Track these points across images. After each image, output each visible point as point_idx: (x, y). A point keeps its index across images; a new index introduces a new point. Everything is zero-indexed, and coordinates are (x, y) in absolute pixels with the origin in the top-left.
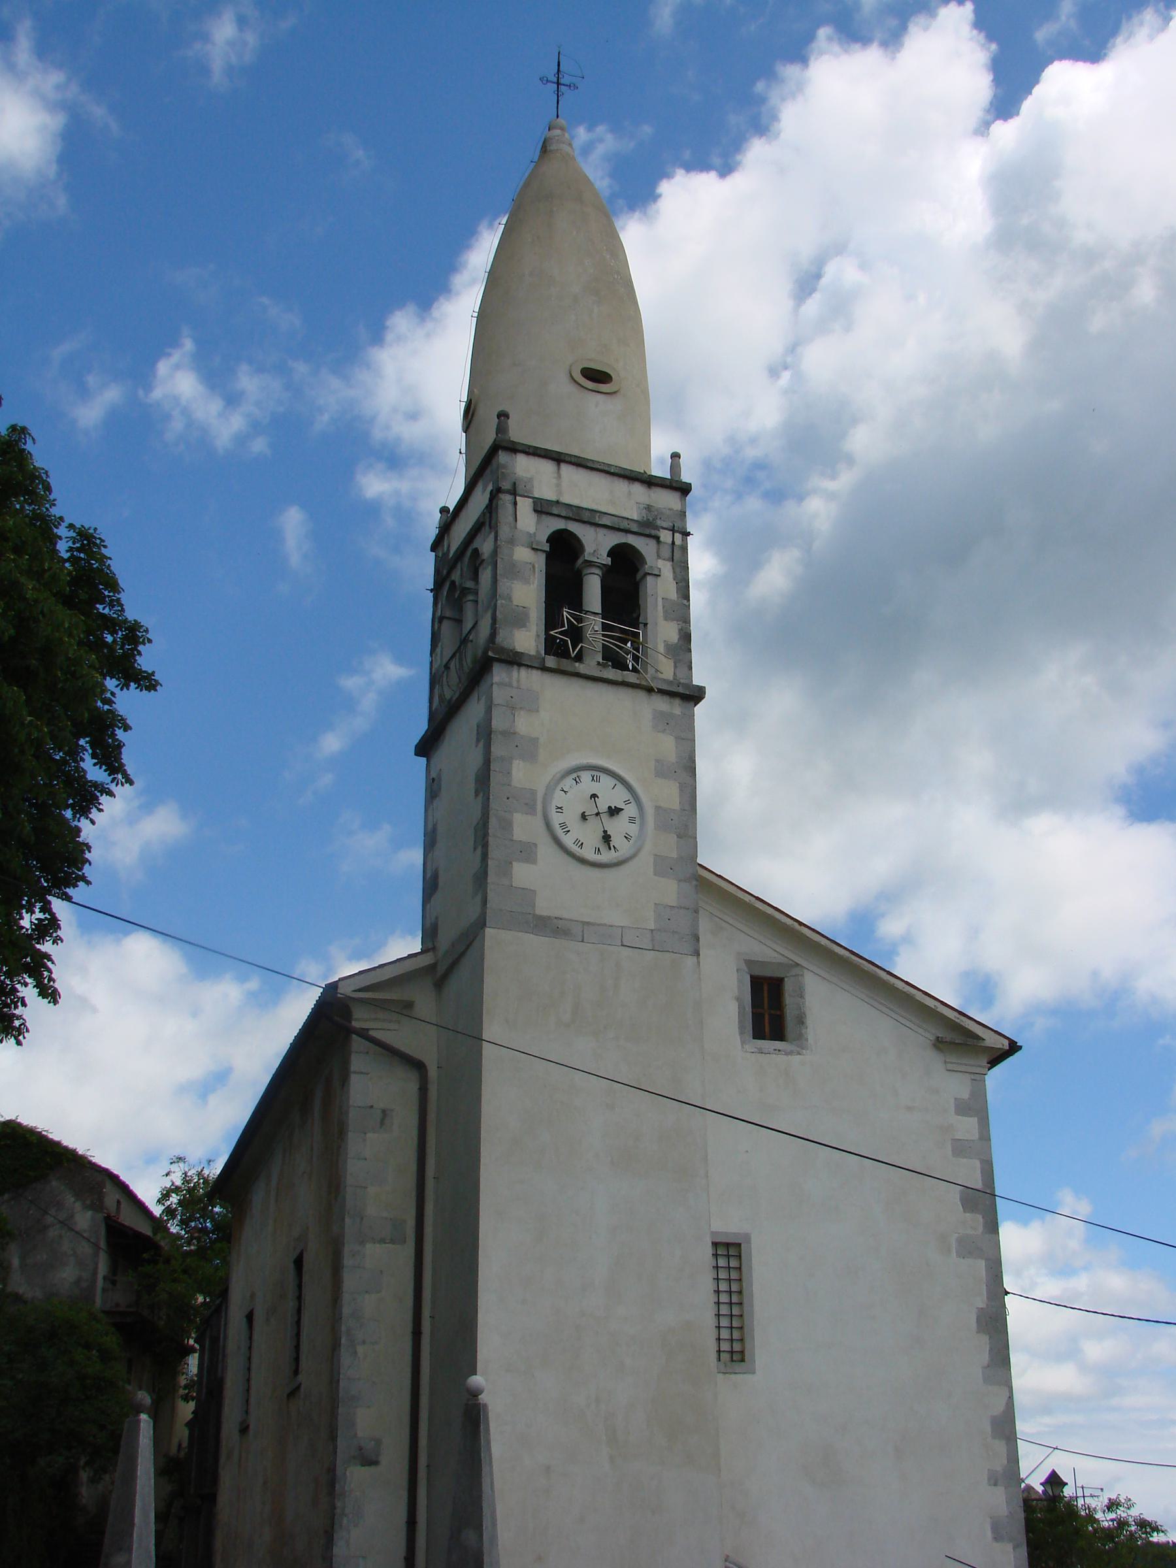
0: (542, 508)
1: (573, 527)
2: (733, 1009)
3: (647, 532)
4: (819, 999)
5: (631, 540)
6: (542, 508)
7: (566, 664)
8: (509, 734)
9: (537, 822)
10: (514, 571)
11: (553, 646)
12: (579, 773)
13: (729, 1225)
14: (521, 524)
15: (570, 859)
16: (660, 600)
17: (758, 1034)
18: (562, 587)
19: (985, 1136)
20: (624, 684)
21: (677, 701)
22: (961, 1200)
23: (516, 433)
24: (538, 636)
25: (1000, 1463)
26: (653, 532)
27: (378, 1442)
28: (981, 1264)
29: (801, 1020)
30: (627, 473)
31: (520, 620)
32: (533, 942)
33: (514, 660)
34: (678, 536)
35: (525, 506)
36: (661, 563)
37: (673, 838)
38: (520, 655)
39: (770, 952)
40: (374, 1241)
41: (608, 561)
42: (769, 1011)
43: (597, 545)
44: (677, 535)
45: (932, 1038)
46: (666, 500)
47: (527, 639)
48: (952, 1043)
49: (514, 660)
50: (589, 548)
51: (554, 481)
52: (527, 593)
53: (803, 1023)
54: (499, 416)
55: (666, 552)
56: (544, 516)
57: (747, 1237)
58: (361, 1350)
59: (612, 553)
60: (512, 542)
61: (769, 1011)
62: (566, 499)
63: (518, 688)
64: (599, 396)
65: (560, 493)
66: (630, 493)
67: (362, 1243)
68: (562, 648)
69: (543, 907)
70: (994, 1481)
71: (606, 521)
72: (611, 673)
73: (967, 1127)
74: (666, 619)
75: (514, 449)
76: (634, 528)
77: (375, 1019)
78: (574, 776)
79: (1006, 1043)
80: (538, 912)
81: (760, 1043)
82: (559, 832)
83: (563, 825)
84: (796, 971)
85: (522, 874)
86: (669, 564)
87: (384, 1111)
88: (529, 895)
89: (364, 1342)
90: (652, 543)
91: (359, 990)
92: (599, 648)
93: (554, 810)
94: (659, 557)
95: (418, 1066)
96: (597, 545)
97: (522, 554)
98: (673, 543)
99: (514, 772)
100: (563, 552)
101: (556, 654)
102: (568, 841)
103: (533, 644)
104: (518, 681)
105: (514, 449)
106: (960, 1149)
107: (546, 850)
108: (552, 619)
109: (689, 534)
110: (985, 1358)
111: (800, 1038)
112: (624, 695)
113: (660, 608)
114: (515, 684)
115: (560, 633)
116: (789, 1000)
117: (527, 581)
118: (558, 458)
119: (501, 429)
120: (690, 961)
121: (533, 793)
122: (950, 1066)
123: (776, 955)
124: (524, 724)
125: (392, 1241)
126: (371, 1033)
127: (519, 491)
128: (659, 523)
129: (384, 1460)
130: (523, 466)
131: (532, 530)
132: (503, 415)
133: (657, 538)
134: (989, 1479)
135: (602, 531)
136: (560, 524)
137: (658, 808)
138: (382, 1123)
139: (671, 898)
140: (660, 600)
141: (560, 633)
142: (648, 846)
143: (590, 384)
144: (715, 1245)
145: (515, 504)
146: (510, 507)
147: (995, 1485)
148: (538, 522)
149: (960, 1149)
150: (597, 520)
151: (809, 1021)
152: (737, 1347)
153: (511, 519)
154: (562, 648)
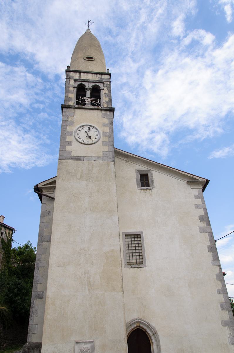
0: (75, 80)
1: (83, 83)
2: (135, 181)
4: (156, 176)
9: (73, 137)
11: (78, 103)
12: (84, 127)
15: (78, 143)
16: (104, 94)
19: (204, 202)
20: (94, 109)
22: (199, 218)
25: (220, 287)
28: (207, 234)
29: (153, 182)
34: (108, 83)
37: (107, 138)
39: (143, 168)
42: (145, 180)
43: (89, 86)
45: (186, 182)
46: (106, 77)
48: (191, 182)
53: (153, 182)
55: (105, 85)
56: (76, 82)
57: (142, 233)
61: (145, 180)
64: (90, 61)
66: (97, 76)
69: (74, 154)
70: (219, 292)
71: (91, 81)
72: (93, 107)
73: (199, 201)
77: (51, 192)
78: (82, 127)
79: (205, 180)
82: (82, 142)
84: (151, 171)
87: (49, 211)
90: (102, 84)
91: (44, 185)
92: (90, 103)
96: (89, 86)
98: (107, 84)
106: (197, 206)
107: (75, 143)
108: (77, 98)
109: (111, 82)
110: (212, 258)
111: (153, 185)
112: (95, 111)
113: (104, 95)
116: (150, 178)
122: (192, 188)
123: (145, 168)
126: (47, 195)
127: (71, 78)
130: (72, 74)
134: (218, 292)
135: (90, 83)
136: (80, 83)
138: (49, 214)
140: (104, 94)
142: (101, 140)
143: (87, 59)
144: (126, 235)
145: (70, 80)
147: (220, 293)
149: (197, 206)
151: (155, 181)
152: (141, 260)
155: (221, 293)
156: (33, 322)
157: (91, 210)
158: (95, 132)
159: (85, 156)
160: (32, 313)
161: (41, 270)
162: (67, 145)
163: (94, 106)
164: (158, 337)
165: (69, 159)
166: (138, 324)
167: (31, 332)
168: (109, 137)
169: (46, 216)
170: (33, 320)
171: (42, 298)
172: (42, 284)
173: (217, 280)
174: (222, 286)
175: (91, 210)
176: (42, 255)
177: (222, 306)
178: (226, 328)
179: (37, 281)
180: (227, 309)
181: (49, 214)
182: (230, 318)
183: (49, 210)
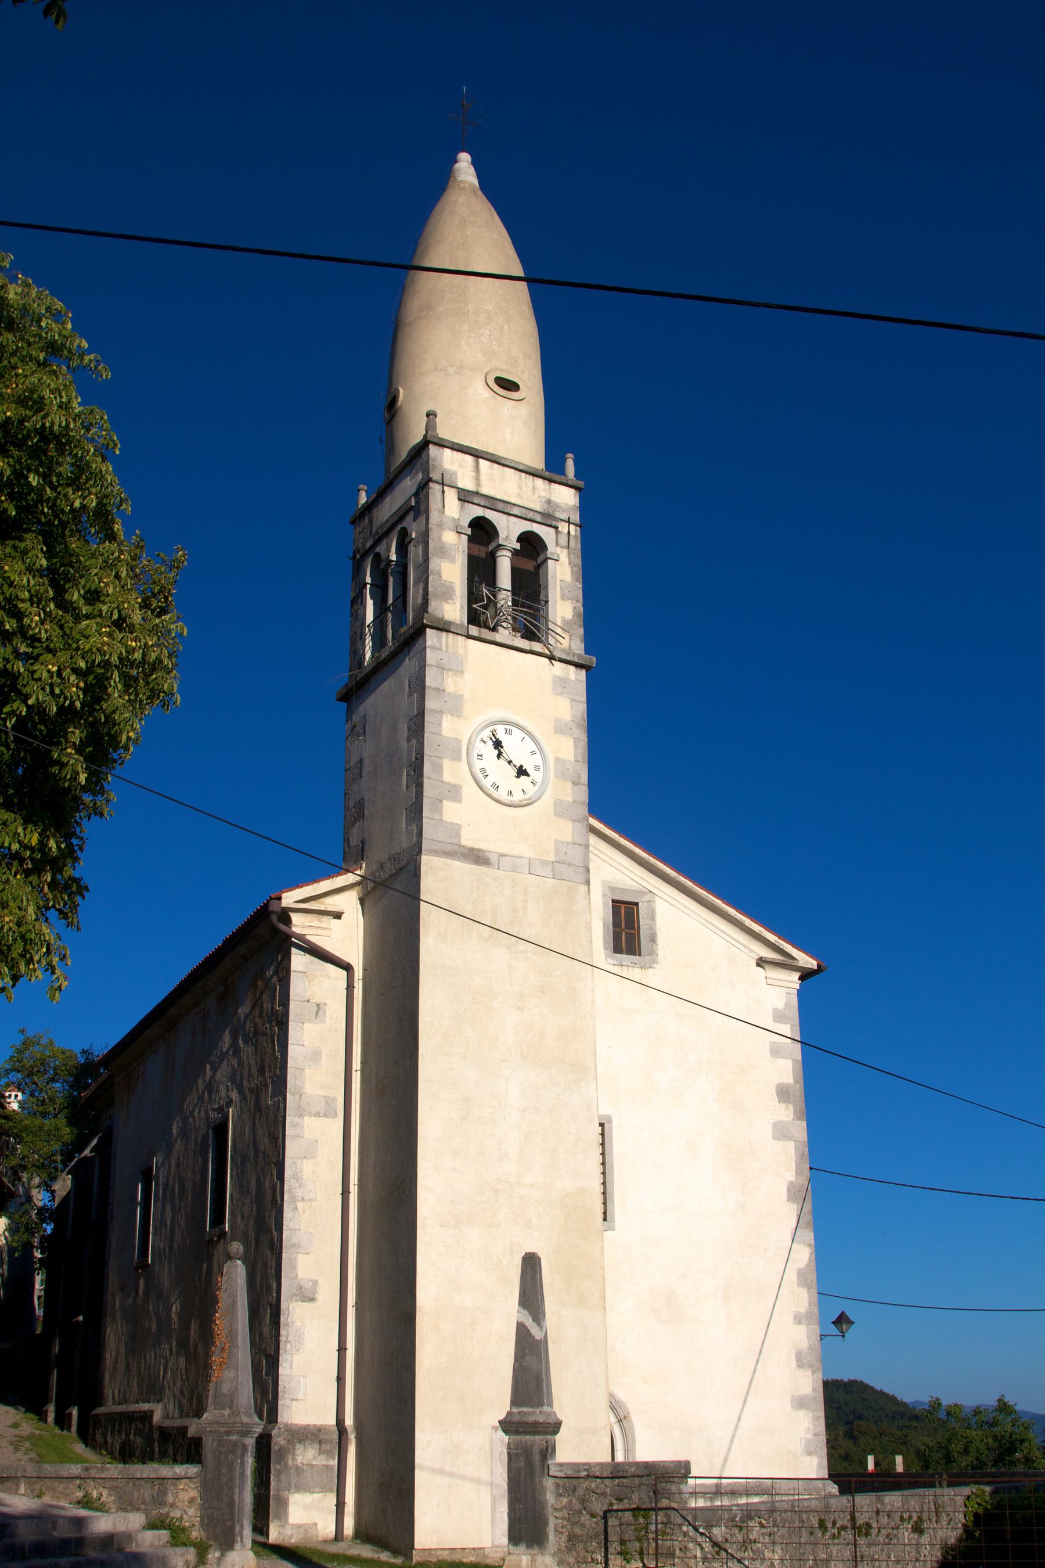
0: (465, 497)
1: (490, 515)
3: (548, 523)
5: (536, 528)
6: (465, 497)
7: (486, 634)
8: (440, 690)
10: (444, 552)
11: (474, 618)
13: (605, 1110)
14: (447, 511)
17: (617, 949)
18: (481, 570)
21: (572, 668)
23: (444, 432)
24: (462, 607)
26: (554, 523)
27: (315, 1283)
29: (653, 939)
30: (532, 471)
31: (447, 594)
32: (460, 867)
33: (444, 627)
35: (451, 496)
36: (558, 550)
38: (450, 623)
40: (310, 1115)
41: (518, 546)
44: (572, 526)
47: (454, 609)
49: (444, 627)
50: (502, 535)
51: (474, 474)
52: (450, 571)
54: (428, 415)
55: (563, 540)
58: (300, 1205)
59: (520, 539)
60: (440, 526)
62: (485, 490)
63: (447, 652)
65: (478, 484)
67: (301, 1116)
68: (480, 616)
69: (468, 839)
74: (563, 598)
75: (442, 444)
76: (539, 518)
80: (464, 842)
81: (619, 956)
83: (483, 770)
85: (451, 812)
86: (565, 551)
88: (456, 829)
89: (303, 1199)
90: (552, 531)
93: (476, 757)
94: (557, 544)
95: (348, 968)
96: (509, 531)
97: (449, 537)
98: (569, 532)
99: (444, 723)
100: (482, 531)
101: (478, 625)
102: (487, 783)
103: (458, 614)
104: (447, 645)
105: (442, 444)
107: (469, 789)
108: (473, 596)
111: (652, 952)
113: (558, 588)
114: (444, 649)
115: (481, 606)
117: (452, 560)
118: (477, 455)
119: (430, 426)
120: (583, 888)
121: (458, 742)
124: (451, 684)
125: (326, 1116)
128: (559, 515)
129: (320, 1296)
131: (456, 516)
132: (431, 415)
133: (556, 528)
134: (795, 1319)
136: (479, 512)
137: (557, 759)
138: (317, 1013)
139: (568, 837)
141: (481, 606)
145: (443, 492)
146: (439, 495)
147: (800, 1323)
148: (462, 508)
150: (509, 510)
151: (660, 940)
153: (440, 505)
154: (480, 616)
155: (803, 1321)
156: (291, 1367)
157: (522, 1055)
158: (533, 753)
159: (501, 851)
160: (287, 1341)
161: (304, 1212)
162: (446, 799)
163: (530, 640)
164: (632, 1427)
165: (451, 854)
166: (47, 1499)
167: (286, 1396)
168: (574, 783)
169: (310, 1021)
170: (291, 1363)
171: (312, 1299)
172: (310, 1256)
173: (798, 1285)
174: (807, 1304)
175: (522, 1055)
176: (305, 1161)
177: (799, 1356)
178: (802, 1413)
179: (294, 1246)
180: (811, 1366)
181: (317, 1013)
182: (814, 1390)
183: (317, 1000)
